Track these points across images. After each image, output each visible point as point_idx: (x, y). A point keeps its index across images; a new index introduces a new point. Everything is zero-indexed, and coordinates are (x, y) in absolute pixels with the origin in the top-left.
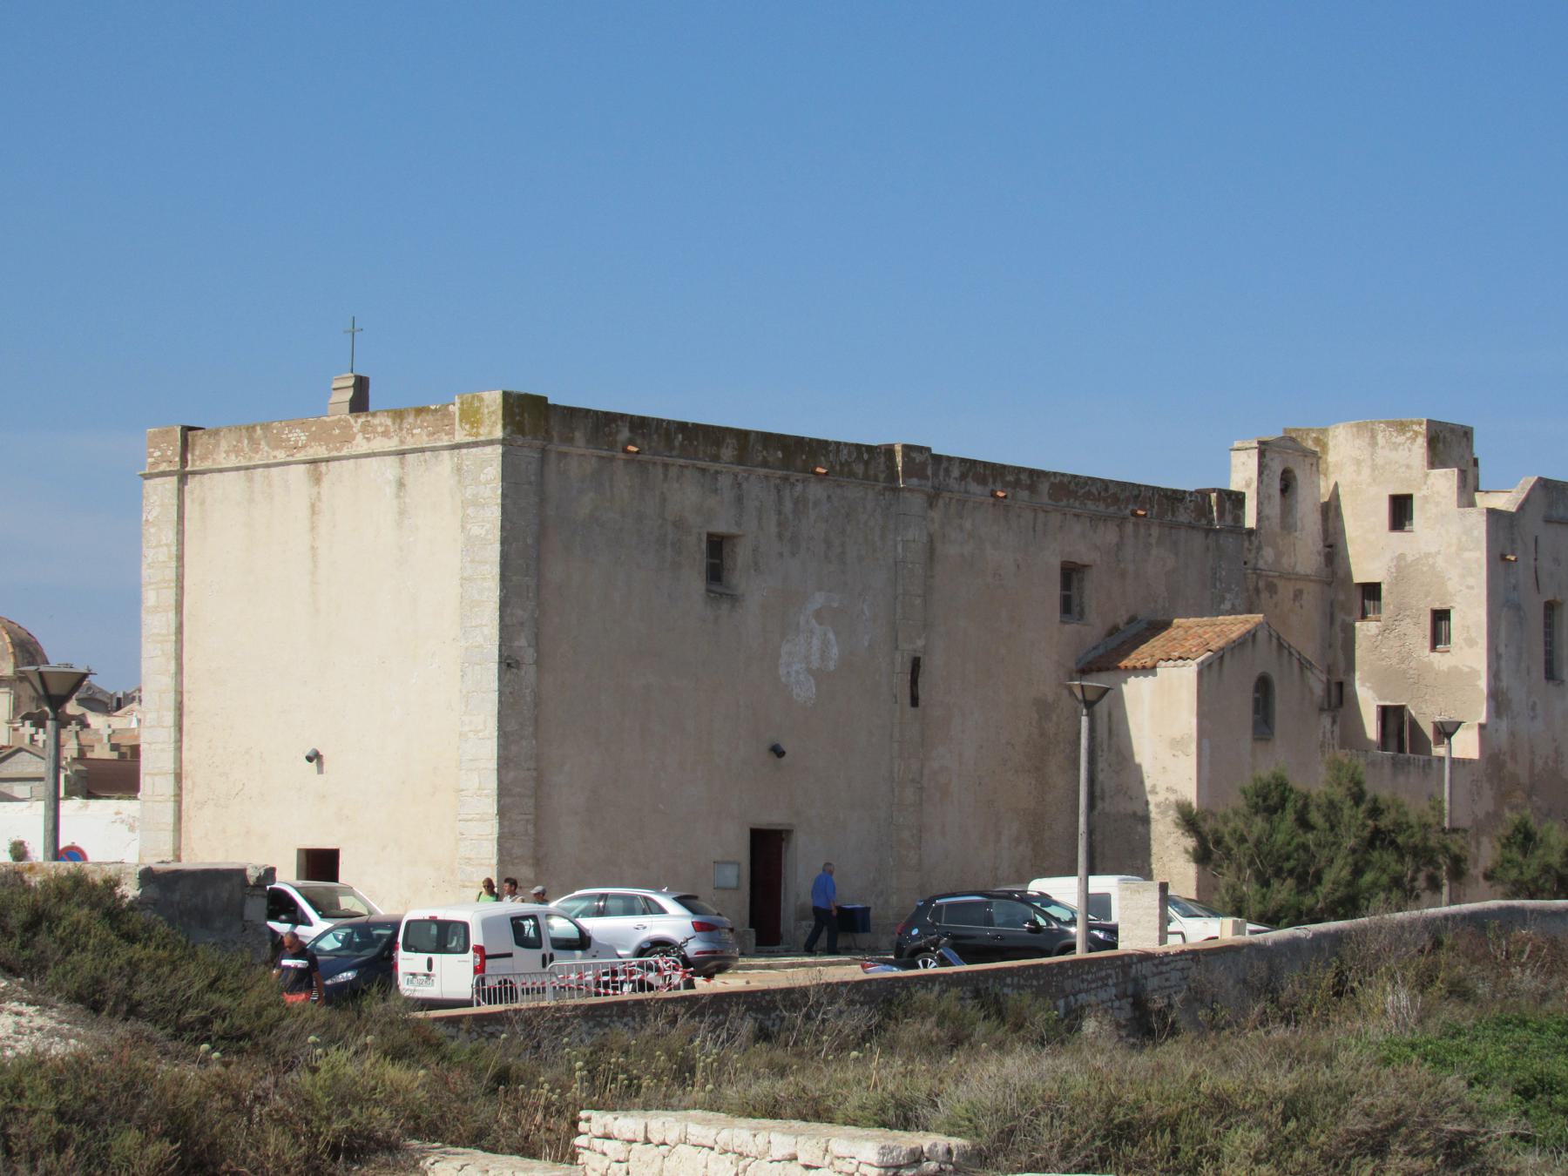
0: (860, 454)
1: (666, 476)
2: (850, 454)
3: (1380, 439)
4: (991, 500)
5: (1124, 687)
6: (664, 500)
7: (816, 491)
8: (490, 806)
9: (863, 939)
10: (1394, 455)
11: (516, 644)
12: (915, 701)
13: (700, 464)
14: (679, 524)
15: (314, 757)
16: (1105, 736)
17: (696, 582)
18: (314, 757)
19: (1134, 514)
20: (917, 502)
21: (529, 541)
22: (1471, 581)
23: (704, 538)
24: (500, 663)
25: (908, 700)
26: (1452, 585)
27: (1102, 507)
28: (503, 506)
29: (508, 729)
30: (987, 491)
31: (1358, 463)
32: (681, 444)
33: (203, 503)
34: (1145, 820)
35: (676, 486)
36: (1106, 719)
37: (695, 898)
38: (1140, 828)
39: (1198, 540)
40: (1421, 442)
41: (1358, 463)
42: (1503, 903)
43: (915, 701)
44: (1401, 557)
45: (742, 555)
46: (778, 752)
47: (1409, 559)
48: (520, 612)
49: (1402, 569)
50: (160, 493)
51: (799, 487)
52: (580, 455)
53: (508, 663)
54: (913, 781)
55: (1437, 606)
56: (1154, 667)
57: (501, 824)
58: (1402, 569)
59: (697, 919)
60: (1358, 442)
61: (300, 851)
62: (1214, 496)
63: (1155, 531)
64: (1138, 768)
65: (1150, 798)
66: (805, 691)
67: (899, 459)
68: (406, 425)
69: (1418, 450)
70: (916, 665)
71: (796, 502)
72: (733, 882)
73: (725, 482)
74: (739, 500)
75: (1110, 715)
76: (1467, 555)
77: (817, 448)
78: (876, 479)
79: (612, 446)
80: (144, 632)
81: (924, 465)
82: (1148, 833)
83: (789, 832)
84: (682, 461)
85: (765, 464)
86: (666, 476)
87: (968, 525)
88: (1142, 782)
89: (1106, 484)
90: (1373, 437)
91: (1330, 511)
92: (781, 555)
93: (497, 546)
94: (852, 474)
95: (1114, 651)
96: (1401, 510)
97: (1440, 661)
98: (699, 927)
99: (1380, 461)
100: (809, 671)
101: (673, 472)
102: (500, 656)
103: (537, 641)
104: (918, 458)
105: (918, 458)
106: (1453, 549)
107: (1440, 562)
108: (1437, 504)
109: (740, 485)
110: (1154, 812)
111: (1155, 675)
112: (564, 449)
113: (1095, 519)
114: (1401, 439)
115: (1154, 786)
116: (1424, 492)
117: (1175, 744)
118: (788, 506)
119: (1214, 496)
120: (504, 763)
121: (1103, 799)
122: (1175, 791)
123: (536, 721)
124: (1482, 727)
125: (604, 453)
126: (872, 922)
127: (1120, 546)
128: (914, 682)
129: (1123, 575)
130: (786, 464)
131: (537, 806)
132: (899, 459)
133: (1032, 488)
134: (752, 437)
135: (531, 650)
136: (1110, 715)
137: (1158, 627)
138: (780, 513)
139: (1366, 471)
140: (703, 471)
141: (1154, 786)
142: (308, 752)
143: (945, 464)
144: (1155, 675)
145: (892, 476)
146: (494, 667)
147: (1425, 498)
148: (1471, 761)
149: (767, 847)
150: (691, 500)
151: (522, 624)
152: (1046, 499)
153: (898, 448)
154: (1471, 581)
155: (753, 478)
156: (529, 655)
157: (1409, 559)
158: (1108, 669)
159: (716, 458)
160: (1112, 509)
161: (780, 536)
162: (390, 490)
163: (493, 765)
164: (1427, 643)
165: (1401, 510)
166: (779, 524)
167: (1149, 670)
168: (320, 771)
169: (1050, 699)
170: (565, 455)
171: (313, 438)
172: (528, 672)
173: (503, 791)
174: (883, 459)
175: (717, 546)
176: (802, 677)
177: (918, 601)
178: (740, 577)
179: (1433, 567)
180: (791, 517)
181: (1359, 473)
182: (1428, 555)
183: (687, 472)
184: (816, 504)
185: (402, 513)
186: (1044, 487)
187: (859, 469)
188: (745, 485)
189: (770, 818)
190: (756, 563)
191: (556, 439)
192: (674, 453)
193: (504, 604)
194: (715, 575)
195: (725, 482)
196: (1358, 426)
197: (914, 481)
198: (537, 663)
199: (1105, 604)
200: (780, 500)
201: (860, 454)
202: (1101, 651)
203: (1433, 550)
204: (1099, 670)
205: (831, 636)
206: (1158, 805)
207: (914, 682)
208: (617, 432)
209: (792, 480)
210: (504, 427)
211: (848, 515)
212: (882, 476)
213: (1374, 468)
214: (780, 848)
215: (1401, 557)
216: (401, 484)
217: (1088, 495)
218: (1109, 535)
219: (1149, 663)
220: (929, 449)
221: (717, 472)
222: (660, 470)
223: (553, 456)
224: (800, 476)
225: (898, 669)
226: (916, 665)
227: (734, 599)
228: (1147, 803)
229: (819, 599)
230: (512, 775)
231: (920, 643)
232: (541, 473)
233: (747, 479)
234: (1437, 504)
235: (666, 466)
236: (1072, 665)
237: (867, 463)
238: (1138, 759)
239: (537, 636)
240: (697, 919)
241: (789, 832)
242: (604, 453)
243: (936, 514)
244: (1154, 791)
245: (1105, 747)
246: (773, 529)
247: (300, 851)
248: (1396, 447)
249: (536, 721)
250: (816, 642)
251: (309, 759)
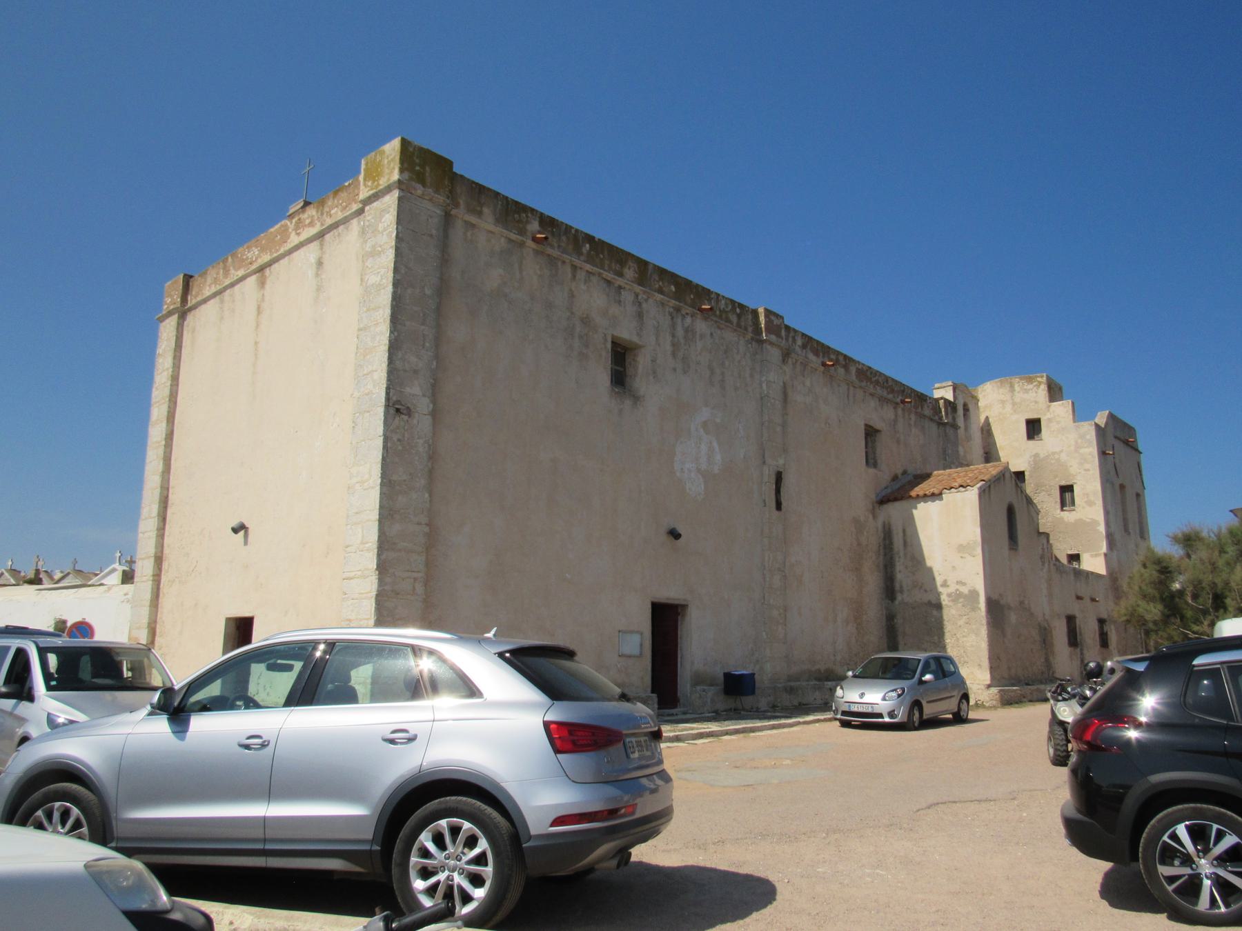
0: (734, 308)
1: (574, 276)
2: (726, 304)
3: (1017, 388)
4: (822, 368)
5: (915, 512)
6: (572, 296)
7: (701, 326)
8: (370, 561)
9: (748, 701)
10: (1026, 396)
11: (408, 390)
12: (779, 506)
13: (606, 274)
14: (586, 321)
15: (239, 528)
16: (901, 547)
17: (602, 375)
18: (239, 528)
19: (903, 402)
20: (774, 354)
21: (428, 292)
22: (1087, 466)
23: (610, 340)
24: (387, 406)
25: (773, 504)
26: (1073, 470)
27: (885, 394)
28: (397, 249)
29: (395, 477)
30: (820, 361)
31: (1003, 402)
32: (589, 253)
33: (193, 331)
34: (939, 607)
35: (583, 287)
36: (901, 534)
37: (569, 654)
38: (935, 612)
39: (934, 427)
40: (1044, 387)
41: (1003, 402)
42: (606, 680)
43: (779, 506)
44: (1036, 455)
45: (642, 362)
46: (674, 534)
47: (1042, 456)
48: (413, 359)
49: (1037, 462)
50: (168, 329)
51: (688, 320)
52: (487, 232)
53: (396, 408)
54: (779, 569)
55: (1063, 483)
56: (941, 494)
57: (381, 581)
58: (1037, 462)
59: (559, 713)
60: (1001, 391)
61: (228, 620)
62: (941, 402)
63: (913, 417)
64: (930, 570)
65: (940, 589)
66: (695, 487)
67: (762, 319)
68: (326, 209)
69: (1042, 392)
70: (779, 478)
71: (686, 331)
72: (636, 652)
73: (627, 297)
74: (640, 315)
75: (904, 531)
76: (1082, 451)
77: (702, 293)
78: (746, 329)
79: (522, 232)
80: (149, 443)
81: (779, 327)
82: (942, 617)
83: (684, 607)
84: (588, 267)
85: (661, 291)
86: (574, 276)
87: (808, 383)
88: (934, 579)
89: (887, 379)
90: (1012, 386)
91: (987, 431)
92: (675, 370)
93: (390, 288)
94: (728, 320)
95: (902, 489)
96: (1034, 428)
97: (1068, 516)
98: (565, 738)
99: (1017, 400)
100: (699, 470)
101: (581, 275)
102: (388, 399)
103: (434, 391)
104: (776, 322)
105: (776, 322)
106: (1072, 448)
107: (1063, 457)
108: (1058, 422)
109: (640, 304)
110: (945, 600)
111: (941, 499)
112: (473, 219)
113: (883, 400)
114: (1030, 386)
115: (945, 581)
116: (1048, 416)
117: (962, 549)
118: (680, 332)
119: (941, 402)
120: (387, 513)
121: (902, 592)
122: (964, 584)
123: (431, 472)
124: (1105, 555)
125: (513, 236)
126: (757, 685)
127: (895, 421)
128: (778, 491)
129: (898, 442)
130: (678, 296)
131: (428, 564)
132: (762, 319)
133: (846, 367)
134: (650, 267)
135: (426, 401)
136: (904, 531)
137: (923, 477)
138: (673, 336)
139: (1009, 408)
140: (609, 282)
141: (945, 581)
142: (235, 523)
143: (792, 334)
144: (941, 499)
145: (757, 331)
146: (380, 411)
147: (1050, 420)
148: (1099, 576)
149: (666, 620)
150: (605, 308)
151: (416, 372)
152: (854, 378)
153: (761, 310)
154: (1087, 466)
155: (651, 301)
156: (423, 405)
157: (1042, 456)
158: (902, 499)
159: (621, 275)
160: (890, 396)
161: (674, 354)
162: (311, 273)
163: (374, 515)
164: (1058, 506)
165: (1034, 428)
166: (673, 345)
167: (936, 496)
168: (246, 543)
169: (862, 519)
170: (473, 226)
171: (263, 250)
172: (422, 422)
173: (384, 544)
174: (750, 317)
175: (621, 355)
176: (693, 475)
177: (779, 429)
178: (641, 382)
179: (1058, 460)
180: (682, 341)
181: (1004, 408)
182: (1054, 453)
183: (594, 279)
184: (702, 336)
185: (319, 289)
186: (853, 369)
187: (734, 319)
188: (644, 305)
189: (670, 593)
190: (654, 372)
191: (462, 206)
192: (582, 258)
193: (394, 347)
194: (620, 378)
195: (627, 297)
196: (1001, 382)
197: (773, 338)
198: (434, 414)
199: (893, 459)
200: (673, 326)
201: (734, 308)
202: (889, 490)
203: (1057, 450)
204: (896, 500)
205: (715, 444)
206: (949, 595)
207: (778, 491)
208: (527, 222)
209: (683, 312)
210: (402, 171)
211: (726, 352)
212: (750, 329)
213: (1014, 404)
214: (676, 621)
215: (1036, 455)
216: (320, 263)
217: (877, 382)
218: (888, 412)
219: (936, 492)
220: (782, 318)
221: (620, 287)
222: (568, 269)
223: (459, 224)
224: (690, 310)
225: (766, 479)
226: (779, 478)
227: (636, 399)
228: (939, 594)
229: (705, 414)
230: (397, 528)
231: (781, 462)
232: (446, 236)
233: (646, 300)
234: (1058, 422)
235: (574, 268)
236: (873, 497)
237: (739, 316)
238: (929, 563)
239: (434, 386)
240: (559, 713)
241: (684, 607)
242: (513, 236)
243: (788, 369)
244: (945, 584)
245: (902, 554)
246: (669, 348)
247: (228, 620)
248: (1027, 391)
249: (431, 472)
250: (704, 447)
251: (235, 530)
